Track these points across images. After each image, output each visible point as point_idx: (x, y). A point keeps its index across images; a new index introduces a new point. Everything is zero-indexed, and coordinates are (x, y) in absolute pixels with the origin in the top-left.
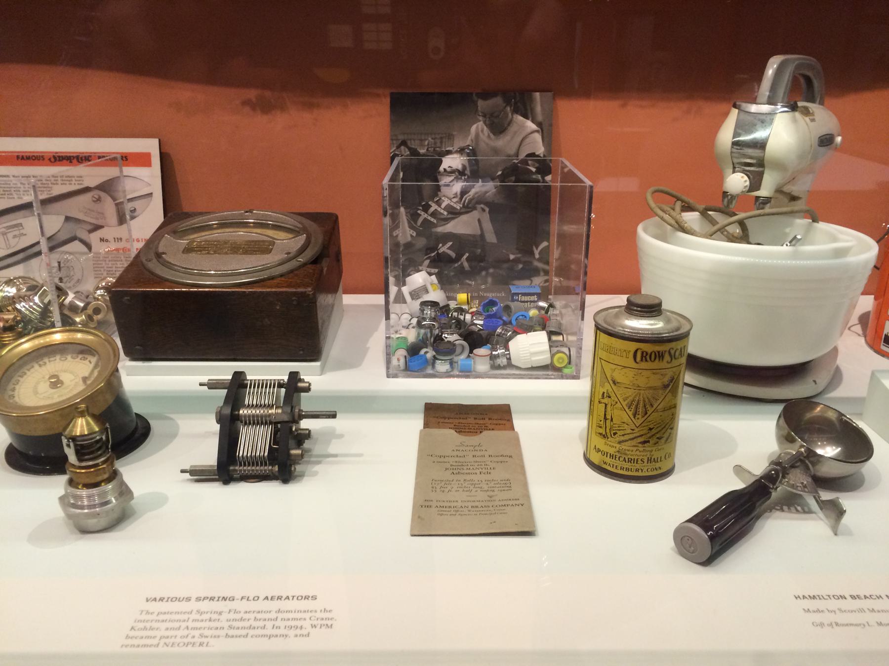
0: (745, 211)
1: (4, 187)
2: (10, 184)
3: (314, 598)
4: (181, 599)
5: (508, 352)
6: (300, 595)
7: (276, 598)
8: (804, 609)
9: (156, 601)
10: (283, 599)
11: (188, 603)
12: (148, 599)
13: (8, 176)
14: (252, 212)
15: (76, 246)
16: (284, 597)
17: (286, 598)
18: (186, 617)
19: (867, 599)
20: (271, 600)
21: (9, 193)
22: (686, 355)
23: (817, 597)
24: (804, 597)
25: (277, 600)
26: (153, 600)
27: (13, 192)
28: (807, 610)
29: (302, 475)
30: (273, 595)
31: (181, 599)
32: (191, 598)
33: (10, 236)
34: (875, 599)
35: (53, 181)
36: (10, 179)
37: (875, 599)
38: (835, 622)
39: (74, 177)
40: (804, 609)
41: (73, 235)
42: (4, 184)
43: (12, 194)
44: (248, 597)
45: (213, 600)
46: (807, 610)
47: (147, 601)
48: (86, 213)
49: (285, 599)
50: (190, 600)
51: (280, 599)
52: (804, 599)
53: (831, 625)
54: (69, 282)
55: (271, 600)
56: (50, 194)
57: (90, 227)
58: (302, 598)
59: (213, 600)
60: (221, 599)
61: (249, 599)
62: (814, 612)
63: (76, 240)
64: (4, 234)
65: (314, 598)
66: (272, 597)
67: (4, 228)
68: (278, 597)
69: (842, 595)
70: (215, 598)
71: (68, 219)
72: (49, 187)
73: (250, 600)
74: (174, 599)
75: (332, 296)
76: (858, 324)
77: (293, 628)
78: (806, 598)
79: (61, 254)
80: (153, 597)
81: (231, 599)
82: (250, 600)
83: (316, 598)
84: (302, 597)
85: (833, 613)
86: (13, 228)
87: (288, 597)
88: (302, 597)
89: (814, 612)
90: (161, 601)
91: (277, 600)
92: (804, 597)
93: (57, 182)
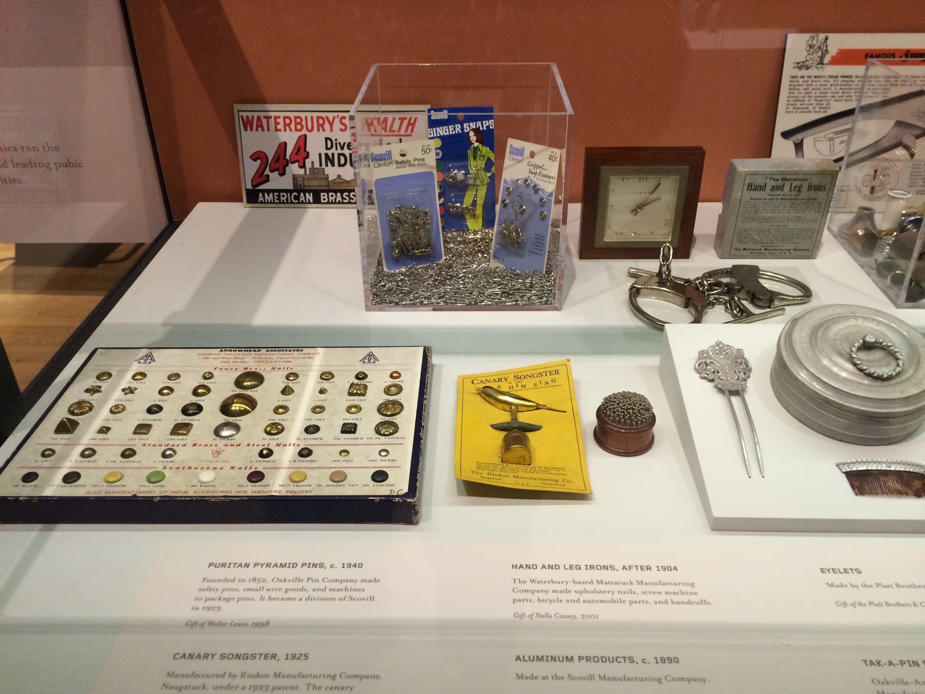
1: (844, 89)
2: (851, 85)
3: (361, 566)
5: (311, 201)
8: (828, 584)
10: (271, 566)
13: (851, 77)
15: (900, 152)
18: (316, 595)
21: (847, 95)
22: (367, 191)
27: (852, 94)
28: (830, 584)
31: (217, 566)
33: (837, 141)
35: (892, 82)
36: (852, 79)
38: (886, 602)
39: (919, 77)
40: (828, 584)
41: (898, 141)
42: (845, 85)
43: (850, 96)
45: (224, 566)
46: (830, 584)
48: (919, 116)
51: (269, 566)
53: (853, 605)
54: (881, 191)
56: (885, 97)
57: (917, 132)
59: (224, 566)
60: (311, 565)
62: (837, 586)
63: (900, 146)
64: (831, 139)
65: (361, 566)
67: (833, 133)
71: (899, 124)
72: (887, 89)
77: (205, 609)
79: (880, 161)
85: (856, 587)
86: (843, 133)
89: (837, 586)
92: (521, 566)
93: (884, 79)
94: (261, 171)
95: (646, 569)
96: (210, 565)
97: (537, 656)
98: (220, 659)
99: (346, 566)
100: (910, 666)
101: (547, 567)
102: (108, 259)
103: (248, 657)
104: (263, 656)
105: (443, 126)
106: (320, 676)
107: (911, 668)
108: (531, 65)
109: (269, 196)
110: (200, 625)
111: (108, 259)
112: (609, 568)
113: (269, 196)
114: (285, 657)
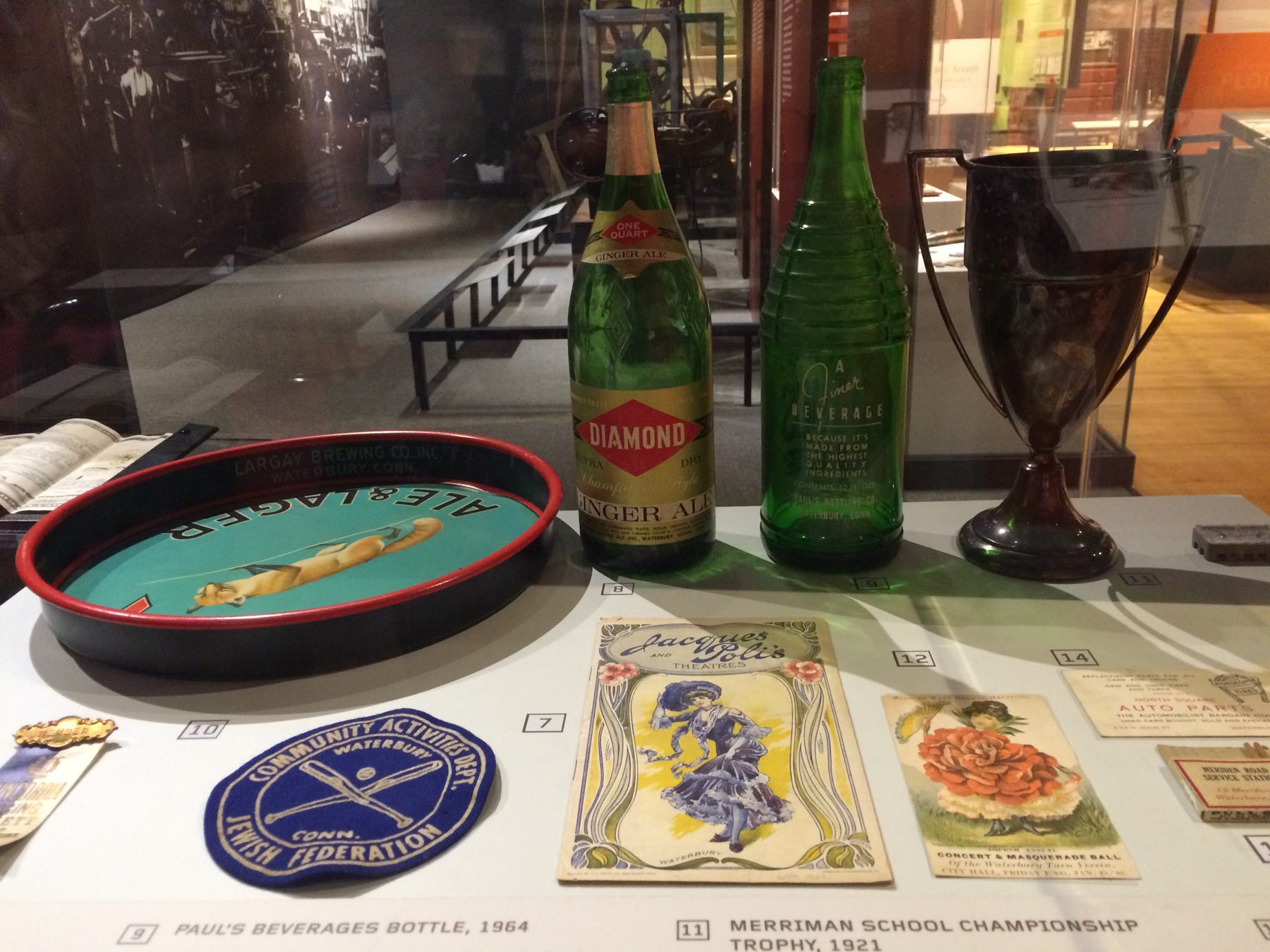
0: (1154, 647)
4: (208, 930)
6: (409, 920)
7: (307, 927)
9: (197, 932)
10: (319, 930)
11: (372, 936)
12: (287, 927)
14: (382, 30)
16: (323, 925)
17: (325, 929)
19: (998, 931)
20: (354, 931)
23: (1124, 926)
24: (996, 925)
25: (308, 931)
26: (191, 931)
29: (1064, 835)
30: (359, 920)
31: (208, 930)
32: (243, 925)
34: (971, 930)
37: (971, 930)
44: (444, 924)
45: (315, 931)
47: (524, 926)
49: (322, 932)
50: (242, 930)
52: (993, 928)
55: (354, 931)
58: (404, 926)
59: (315, 931)
61: (447, 928)
66: (356, 926)
68: (311, 925)
69: (1073, 921)
70: (319, 925)
73: (448, 932)
74: (408, 928)
75: (817, 516)
76: (700, 243)
78: (1000, 927)
80: (192, 924)
81: (341, 929)
82: (448, 932)
83: (376, 929)
84: (403, 930)
87: (331, 925)
88: (403, 930)
90: (312, 932)
91: (308, 931)
92: (996, 925)
94: (23, 515)
95: (763, 927)
96: (180, 929)
97: (904, 929)
98: (377, 924)
99: (490, 927)
100: (1046, 929)
101: (838, 925)
102: (396, 157)
103: (514, 928)
104: (439, 927)
105: (1084, 36)
106: (423, 924)
107: (1046, 933)
108: (106, 11)
109: (631, 433)
110: (520, 927)
111: (396, 157)
112: (1083, 927)
113: (631, 433)
114: (482, 927)
